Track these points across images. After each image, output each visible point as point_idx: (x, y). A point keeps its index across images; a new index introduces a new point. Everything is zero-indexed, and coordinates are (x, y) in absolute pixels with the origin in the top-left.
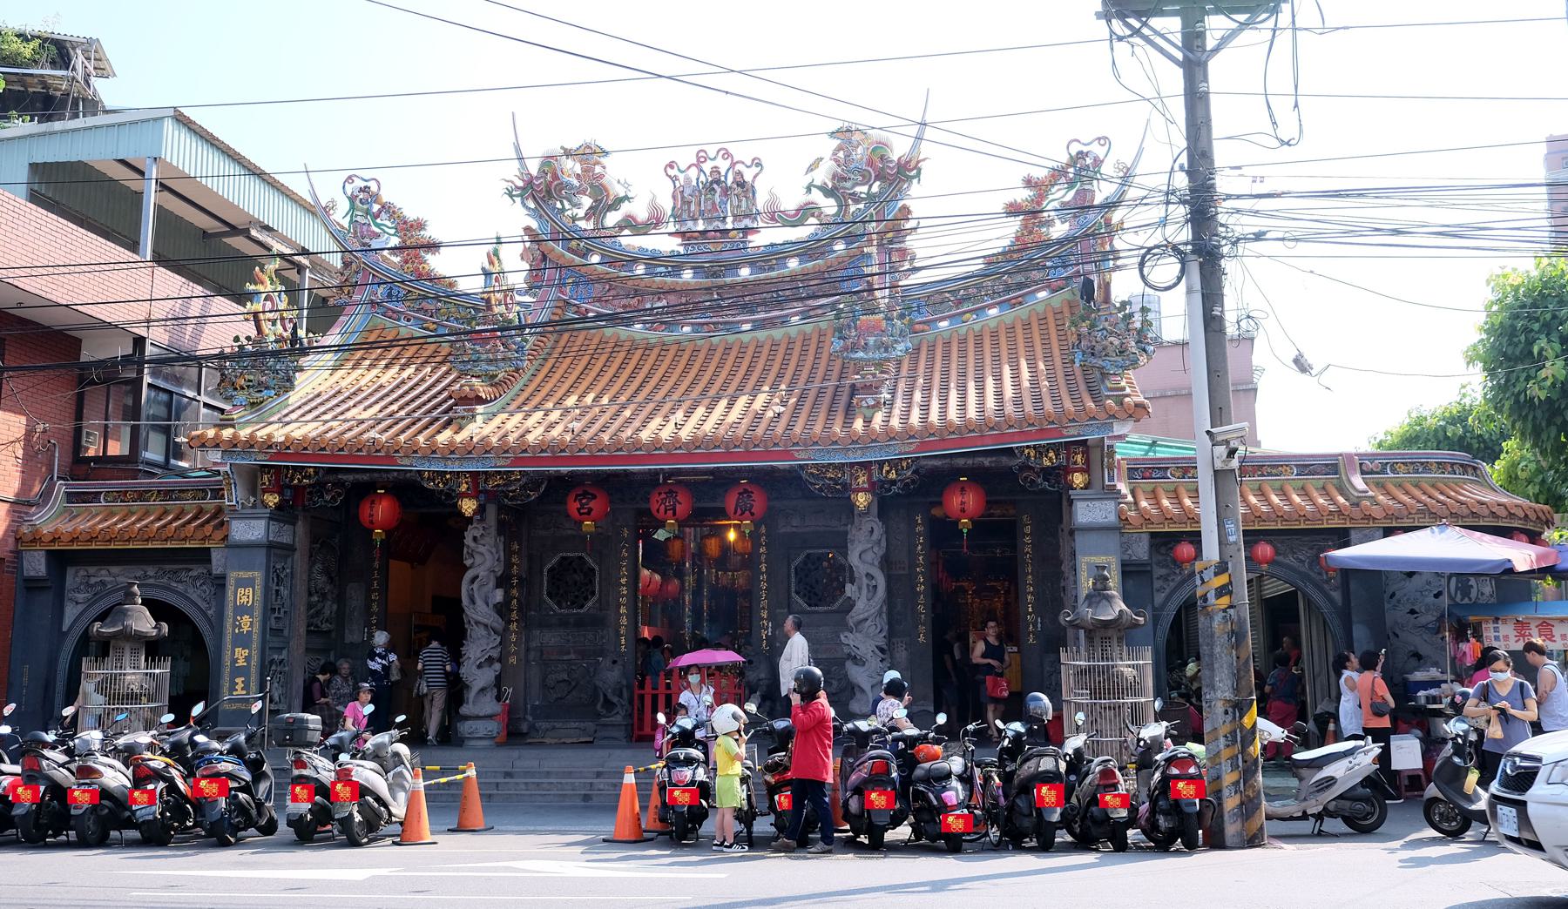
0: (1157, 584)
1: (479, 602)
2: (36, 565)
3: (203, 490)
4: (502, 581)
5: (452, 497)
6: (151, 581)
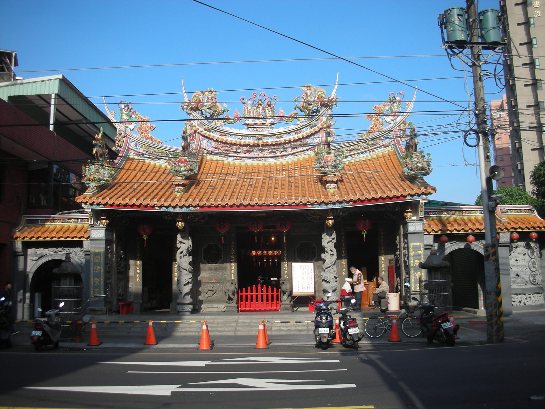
3: (78, 219)
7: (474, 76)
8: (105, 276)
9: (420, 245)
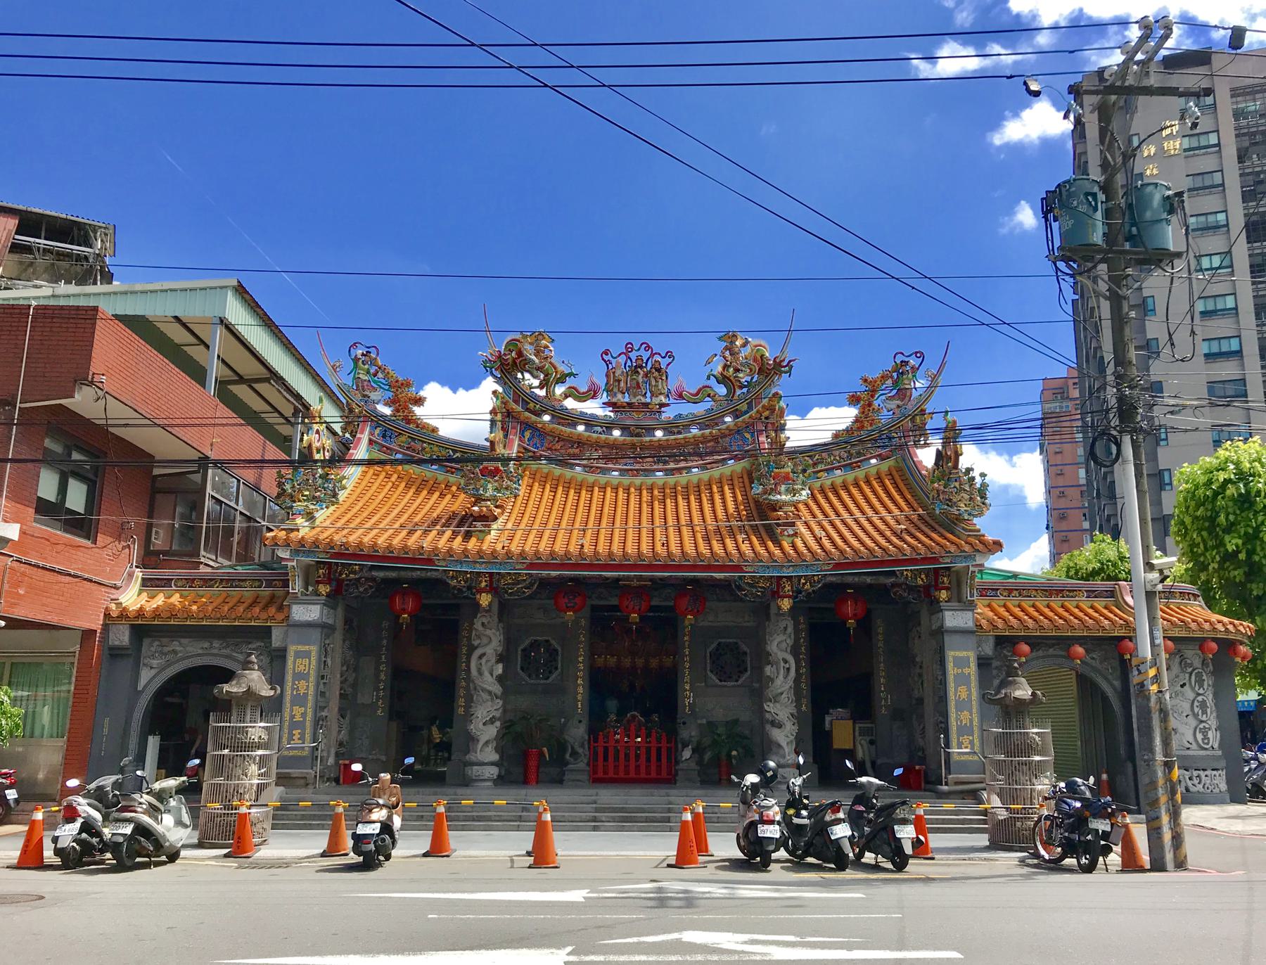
0: (995, 672)
1: (486, 674)
2: (122, 636)
4: (501, 659)
5: (473, 589)
6: (215, 651)
7: (1074, 321)
8: (317, 702)
9: (968, 658)
